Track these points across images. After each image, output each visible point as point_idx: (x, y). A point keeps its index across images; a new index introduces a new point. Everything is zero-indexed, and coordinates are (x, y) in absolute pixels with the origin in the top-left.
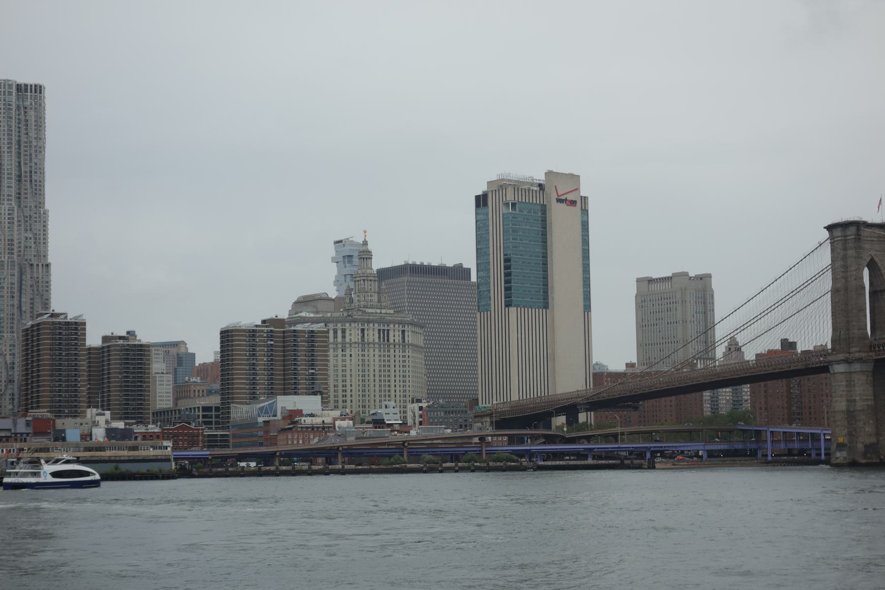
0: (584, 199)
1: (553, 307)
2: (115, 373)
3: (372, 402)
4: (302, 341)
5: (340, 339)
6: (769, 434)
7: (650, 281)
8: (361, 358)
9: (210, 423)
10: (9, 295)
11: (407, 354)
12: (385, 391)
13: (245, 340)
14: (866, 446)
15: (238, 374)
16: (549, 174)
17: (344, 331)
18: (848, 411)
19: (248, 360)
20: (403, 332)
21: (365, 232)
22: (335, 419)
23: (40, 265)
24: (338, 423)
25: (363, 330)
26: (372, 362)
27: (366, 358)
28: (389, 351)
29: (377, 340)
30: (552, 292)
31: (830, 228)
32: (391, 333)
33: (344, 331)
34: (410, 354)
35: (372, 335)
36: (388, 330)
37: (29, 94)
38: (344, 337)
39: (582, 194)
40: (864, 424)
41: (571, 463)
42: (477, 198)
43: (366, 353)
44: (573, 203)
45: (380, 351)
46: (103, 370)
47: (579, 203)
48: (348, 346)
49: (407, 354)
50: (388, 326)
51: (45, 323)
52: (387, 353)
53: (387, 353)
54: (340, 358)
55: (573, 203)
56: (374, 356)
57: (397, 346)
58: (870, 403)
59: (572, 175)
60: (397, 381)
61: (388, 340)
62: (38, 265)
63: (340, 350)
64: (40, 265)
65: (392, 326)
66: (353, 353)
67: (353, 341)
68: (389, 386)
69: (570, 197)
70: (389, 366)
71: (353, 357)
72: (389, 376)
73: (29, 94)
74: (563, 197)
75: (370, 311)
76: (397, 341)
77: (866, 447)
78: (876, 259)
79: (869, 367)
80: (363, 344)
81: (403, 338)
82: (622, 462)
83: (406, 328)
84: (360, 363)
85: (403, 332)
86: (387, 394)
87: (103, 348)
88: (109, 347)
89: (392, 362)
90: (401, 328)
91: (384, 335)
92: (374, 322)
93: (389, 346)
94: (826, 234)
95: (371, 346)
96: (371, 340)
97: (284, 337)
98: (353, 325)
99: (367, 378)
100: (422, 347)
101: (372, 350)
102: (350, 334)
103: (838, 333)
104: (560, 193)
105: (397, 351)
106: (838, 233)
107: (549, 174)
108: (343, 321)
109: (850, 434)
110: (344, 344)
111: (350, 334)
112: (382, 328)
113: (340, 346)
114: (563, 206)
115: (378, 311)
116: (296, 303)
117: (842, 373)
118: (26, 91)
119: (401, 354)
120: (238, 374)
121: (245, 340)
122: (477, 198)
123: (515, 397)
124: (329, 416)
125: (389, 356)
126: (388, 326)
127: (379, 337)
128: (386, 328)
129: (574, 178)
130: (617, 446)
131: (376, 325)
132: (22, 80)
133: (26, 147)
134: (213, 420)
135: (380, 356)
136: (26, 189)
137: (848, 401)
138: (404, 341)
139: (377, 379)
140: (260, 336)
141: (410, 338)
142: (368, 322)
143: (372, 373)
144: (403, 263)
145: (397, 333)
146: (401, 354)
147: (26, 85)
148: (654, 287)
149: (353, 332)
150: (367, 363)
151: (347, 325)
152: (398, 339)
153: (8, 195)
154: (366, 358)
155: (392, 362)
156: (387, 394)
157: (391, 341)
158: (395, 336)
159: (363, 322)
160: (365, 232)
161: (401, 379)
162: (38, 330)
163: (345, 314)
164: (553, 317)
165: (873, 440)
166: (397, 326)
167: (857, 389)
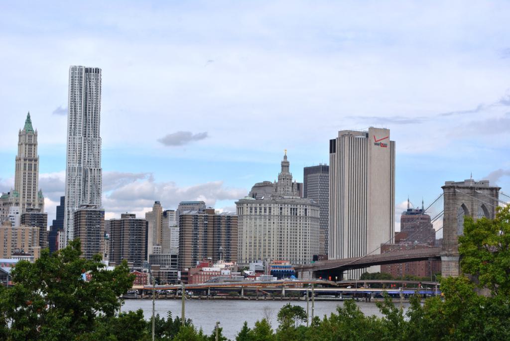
0: (393, 144)
2: (127, 235)
4: (223, 222)
5: (267, 213)
6: (436, 286)
8: (279, 224)
9: (176, 264)
10: (78, 184)
11: (307, 223)
12: (293, 244)
13: (192, 221)
15: (187, 239)
17: (270, 209)
19: (193, 231)
20: (306, 210)
22: (222, 269)
23: (96, 169)
24: (222, 271)
25: (281, 208)
27: (283, 225)
28: (296, 221)
29: (289, 214)
32: (298, 210)
33: (270, 209)
34: (309, 223)
35: (286, 211)
36: (297, 209)
37: (92, 74)
38: (270, 212)
39: (391, 139)
42: (331, 141)
44: (384, 146)
45: (291, 220)
46: (121, 235)
47: (389, 146)
49: (307, 223)
51: (83, 211)
52: (295, 222)
53: (295, 222)
54: (267, 224)
55: (384, 146)
56: (287, 224)
57: (302, 218)
61: (296, 215)
62: (95, 170)
63: (268, 220)
64: (96, 169)
65: (299, 206)
66: (275, 222)
67: (275, 214)
68: (296, 241)
69: (383, 142)
70: (296, 229)
72: (296, 235)
73: (92, 74)
74: (379, 142)
76: (302, 215)
78: (466, 204)
80: (281, 216)
81: (306, 213)
83: (307, 208)
84: (279, 227)
85: (306, 210)
86: (295, 245)
87: (121, 221)
88: (124, 220)
90: (304, 207)
92: (288, 204)
93: (296, 218)
94: (442, 191)
95: (286, 217)
96: (286, 214)
97: (214, 219)
98: (276, 205)
100: (318, 218)
101: (286, 220)
102: (274, 211)
104: (377, 140)
105: (302, 221)
108: (270, 203)
110: (270, 215)
111: (274, 211)
112: (293, 207)
115: (291, 197)
116: (255, 187)
118: (91, 72)
119: (304, 222)
120: (187, 239)
121: (192, 221)
122: (331, 141)
123: (346, 257)
124: (219, 267)
127: (291, 213)
128: (295, 207)
130: (355, 290)
131: (289, 205)
132: (88, 66)
133: (90, 101)
134: (177, 262)
135: (291, 223)
136: (89, 127)
138: (306, 215)
139: (289, 237)
140: (200, 219)
141: (309, 214)
144: (319, 165)
145: (302, 210)
146: (304, 222)
147: (91, 69)
149: (275, 209)
151: (272, 205)
152: (302, 214)
153: (79, 131)
154: (283, 225)
155: (298, 227)
156: (295, 245)
157: (298, 215)
158: (300, 212)
161: (304, 237)
162: (80, 214)
163: (272, 199)
166: (302, 206)
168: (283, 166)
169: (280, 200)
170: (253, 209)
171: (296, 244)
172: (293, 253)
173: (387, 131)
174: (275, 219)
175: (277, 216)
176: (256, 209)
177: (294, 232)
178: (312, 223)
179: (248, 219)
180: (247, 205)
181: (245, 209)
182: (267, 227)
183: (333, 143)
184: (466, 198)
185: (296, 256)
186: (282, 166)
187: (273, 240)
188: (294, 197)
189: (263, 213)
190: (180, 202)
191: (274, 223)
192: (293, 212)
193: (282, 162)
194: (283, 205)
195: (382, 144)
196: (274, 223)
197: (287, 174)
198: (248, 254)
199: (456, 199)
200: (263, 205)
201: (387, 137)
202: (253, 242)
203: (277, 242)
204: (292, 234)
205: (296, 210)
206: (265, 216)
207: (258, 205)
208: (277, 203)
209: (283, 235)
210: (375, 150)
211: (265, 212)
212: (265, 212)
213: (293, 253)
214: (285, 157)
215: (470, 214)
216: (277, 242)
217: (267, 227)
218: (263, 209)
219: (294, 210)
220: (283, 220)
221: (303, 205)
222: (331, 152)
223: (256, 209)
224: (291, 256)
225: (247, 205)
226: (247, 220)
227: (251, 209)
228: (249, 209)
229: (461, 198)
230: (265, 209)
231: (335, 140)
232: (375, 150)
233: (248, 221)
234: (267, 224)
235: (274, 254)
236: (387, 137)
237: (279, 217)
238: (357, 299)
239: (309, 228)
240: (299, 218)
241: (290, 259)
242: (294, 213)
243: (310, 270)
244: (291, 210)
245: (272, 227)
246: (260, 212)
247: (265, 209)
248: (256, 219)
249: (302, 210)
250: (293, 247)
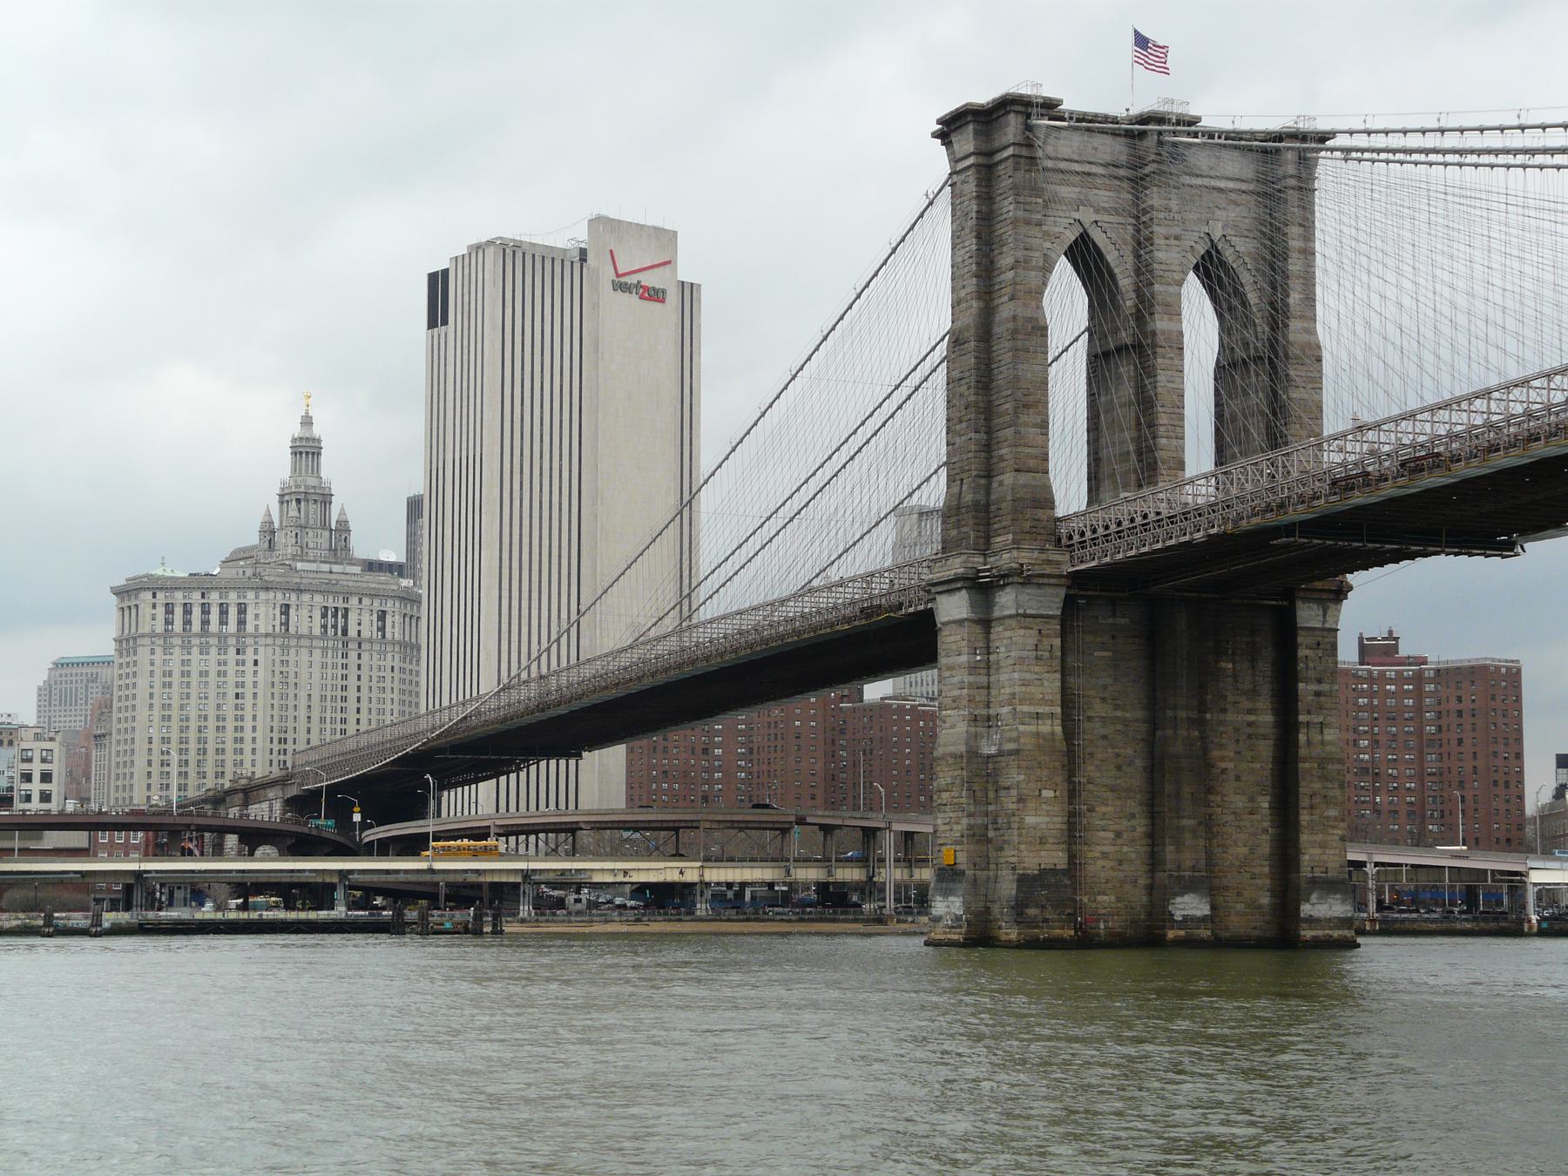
0: (689, 291)
5: (232, 627)
14: (1023, 881)
17: (242, 609)
18: (973, 753)
25: (286, 609)
26: (304, 675)
27: (292, 669)
31: (949, 127)
33: (242, 609)
35: (305, 619)
36: (346, 610)
38: (242, 622)
39: (685, 273)
40: (1021, 800)
41: (268, 915)
42: (433, 278)
43: (292, 658)
44: (655, 295)
47: (673, 297)
50: (346, 600)
54: (231, 668)
55: (655, 295)
58: (1045, 728)
59: (659, 233)
61: (345, 632)
63: (232, 651)
65: (354, 601)
67: (262, 630)
69: (649, 279)
71: (260, 668)
76: (365, 634)
77: (1025, 882)
78: (1098, 237)
79: (1050, 602)
82: (49, 920)
83: (389, 606)
84: (277, 679)
91: (335, 618)
93: (345, 644)
94: (937, 162)
96: (304, 630)
98: (263, 595)
99: (291, 713)
103: (956, 489)
105: (365, 656)
106: (966, 142)
107: (600, 224)
108: (241, 589)
109: (978, 837)
112: (331, 604)
113: (232, 641)
114: (632, 299)
115: (326, 567)
117: (960, 622)
119: (375, 662)
122: (433, 278)
126: (346, 600)
128: (341, 605)
129: (667, 238)
130: (423, 865)
137: (975, 719)
142: (300, 591)
145: (366, 617)
150: (291, 680)
151: (251, 595)
157: (352, 632)
158: (362, 621)
163: (249, 572)
165: (1055, 857)
166: (366, 601)
167: (1004, 677)
168: (297, 452)
169: (281, 575)
170: (179, 611)
173: (667, 238)
174: (261, 650)
175: (267, 635)
176: (187, 609)
178: (407, 666)
179: (158, 650)
180: (154, 596)
181: (145, 610)
182: (231, 678)
183: (438, 284)
184: (1104, 197)
187: (254, 728)
189: (214, 626)
190: (54, 659)
192: (330, 621)
193: (294, 440)
195: (646, 289)
196: (256, 663)
197: (311, 481)
198: (155, 780)
199: (1036, 190)
200: (214, 597)
201: (669, 263)
202: (175, 736)
203: (269, 746)
205: (345, 616)
206: (223, 637)
207: (197, 596)
208: (267, 589)
210: (616, 316)
211: (223, 622)
212: (223, 622)
214: (307, 421)
215: (1129, 303)
216: (269, 746)
217: (231, 678)
218: (215, 611)
219: (335, 616)
222: (432, 324)
223: (187, 609)
225: (154, 596)
226: (153, 652)
227: (169, 609)
228: (160, 611)
229: (1067, 192)
230: (224, 612)
231: (445, 272)
232: (616, 316)
233: (159, 656)
234: (231, 668)
236: (669, 263)
238: (424, 917)
239: (395, 696)
242: (335, 627)
243: (271, 794)
244: (324, 616)
245: (249, 679)
246: (205, 623)
247: (224, 612)
248: (186, 647)
249: (366, 617)
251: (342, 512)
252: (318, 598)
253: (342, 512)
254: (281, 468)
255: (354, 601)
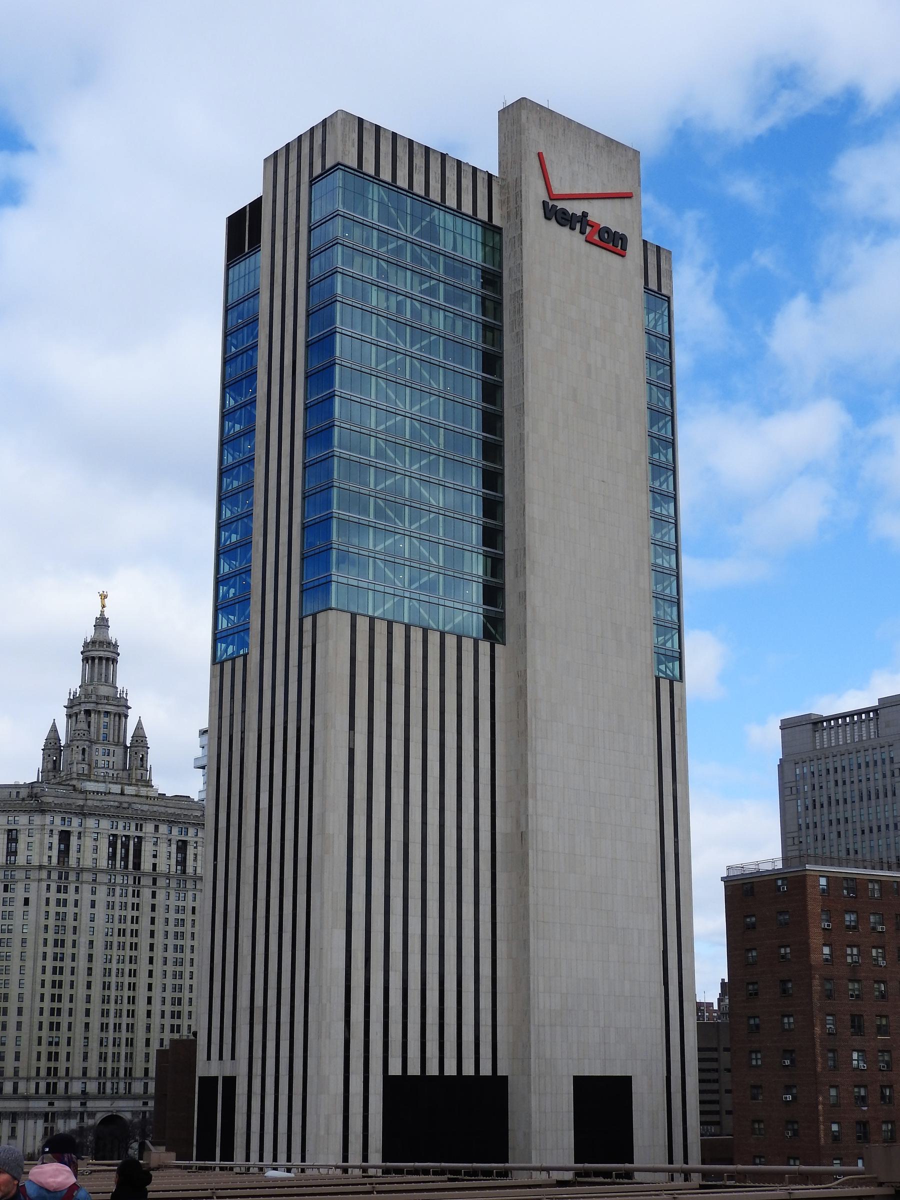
1: (522, 631)
3: (79, 1029)
7: (816, 723)
8: (53, 909)
16: (519, 119)
20: (182, 847)
21: (104, 597)
25: (65, 837)
29: (103, 863)
30: (521, 571)
32: (147, 849)
44: (612, 241)
45: (111, 892)
48: (20, 875)
52: (130, 900)
53: (130, 900)
55: (612, 241)
57: (161, 882)
60: (158, 973)
61: (137, 866)
65: (149, 828)
67: (35, 862)
69: (602, 214)
70: (135, 933)
74: (575, 208)
75: (90, 786)
76: (162, 868)
80: (64, 870)
84: (51, 922)
85: (182, 847)
86: (125, 1007)
89: (145, 922)
93: (137, 881)
96: (88, 863)
98: (37, 819)
101: (86, 889)
105: (161, 895)
112: (120, 831)
115: (116, 789)
119: (173, 902)
125: (136, 907)
126: (139, 827)
127: (112, 857)
128: (132, 832)
135: (110, 906)
142: (83, 814)
143: (83, 951)
145: (163, 848)
148: (825, 739)
149: (36, 838)
150: (70, 922)
151: (76, 821)
152: (167, 863)
154: (70, 910)
155: (145, 922)
156: (125, 1007)
157: (146, 866)
159: (68, 811)
160: (104, 597)
164: (522, 676)
166: (163, 829)
171: (132, 1000)
172: (117, 1027)
174: (34, 886)
175: (41, 867)
177: (121, 946)
185: (130, 1057)
186: (86, 660)
188: (129, 790)
191: (26, 902)
193: (86, 645)
194: (192, 831)
196: (26, 902)
197: (104, 690)
204: (115, 952)
208: (43, 812)
209: (65, 1013)
213: (117, 1027)
214: (102, 623)
220: (72, 888)
221: (171, 823)
224: (103, 1057)
225: (157, 827)
235: (26, 1004)
237: (55, 875)
240: (146, 881)
241: (102, 1073)
244: (112, 844)
249: (163, 848)
250: (120, 986)
251: (139, 727)
252: (105, 824)
253: (139, 727)
254: (71, 678)
255: (149, 828)
